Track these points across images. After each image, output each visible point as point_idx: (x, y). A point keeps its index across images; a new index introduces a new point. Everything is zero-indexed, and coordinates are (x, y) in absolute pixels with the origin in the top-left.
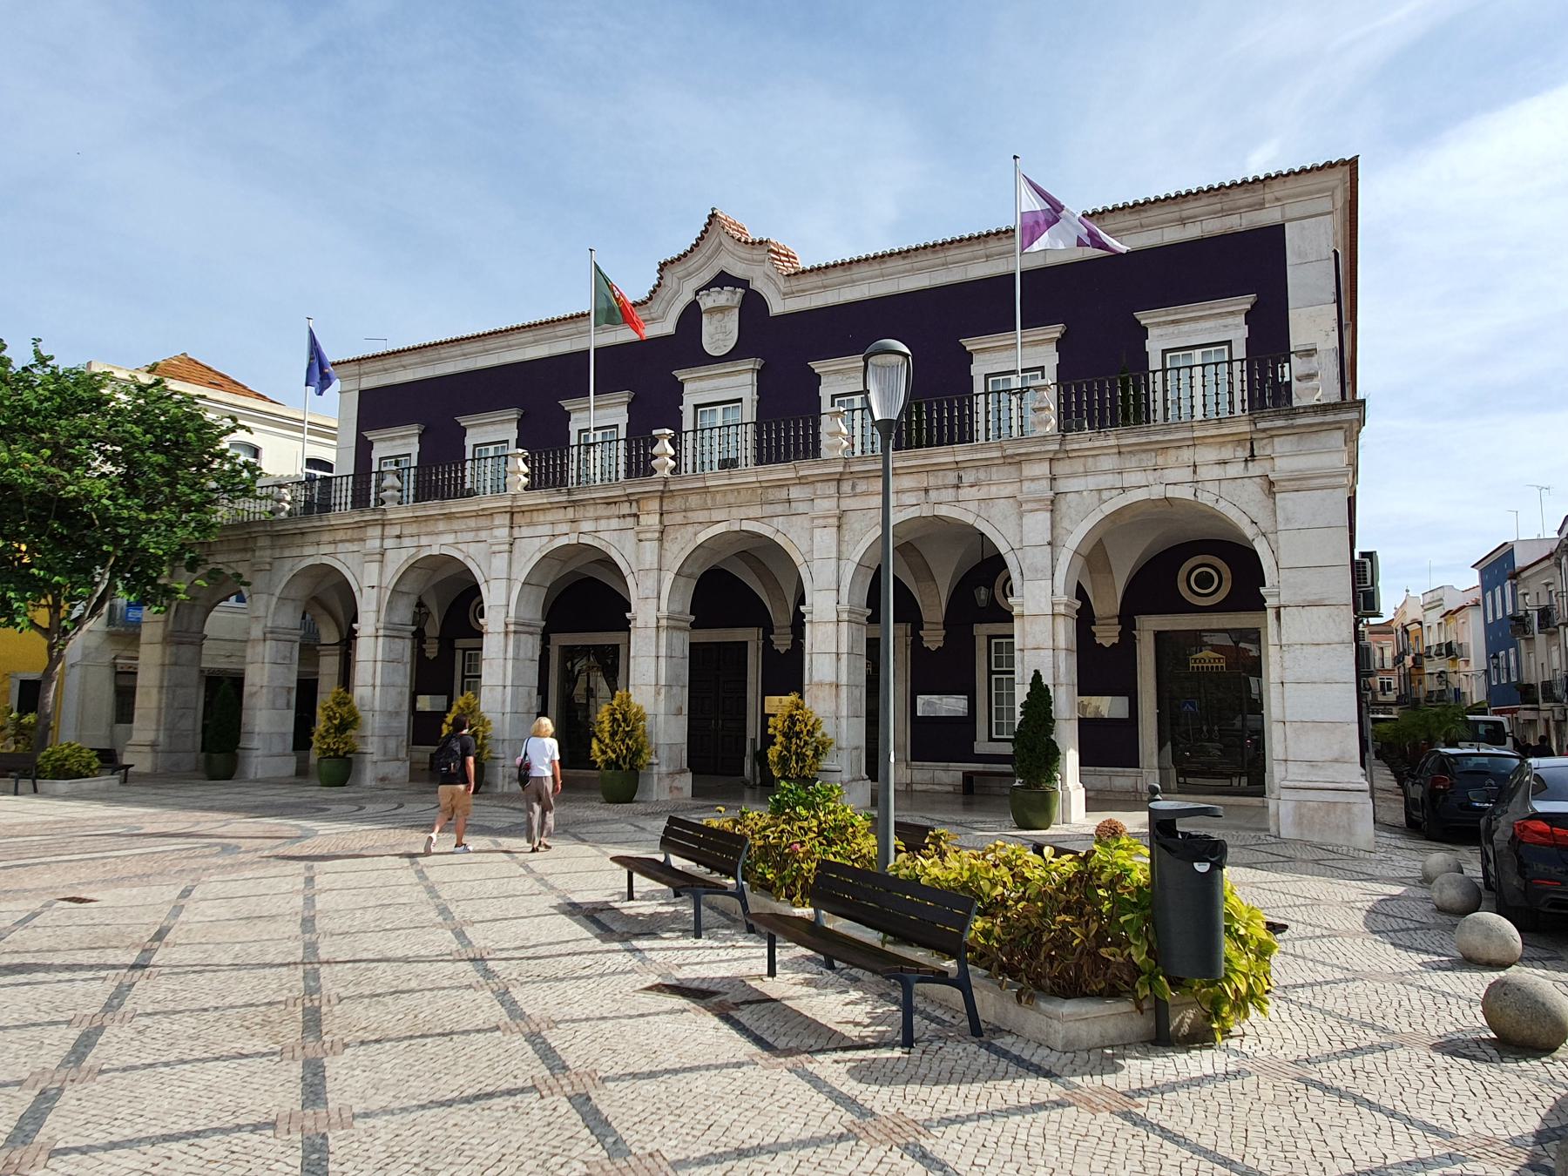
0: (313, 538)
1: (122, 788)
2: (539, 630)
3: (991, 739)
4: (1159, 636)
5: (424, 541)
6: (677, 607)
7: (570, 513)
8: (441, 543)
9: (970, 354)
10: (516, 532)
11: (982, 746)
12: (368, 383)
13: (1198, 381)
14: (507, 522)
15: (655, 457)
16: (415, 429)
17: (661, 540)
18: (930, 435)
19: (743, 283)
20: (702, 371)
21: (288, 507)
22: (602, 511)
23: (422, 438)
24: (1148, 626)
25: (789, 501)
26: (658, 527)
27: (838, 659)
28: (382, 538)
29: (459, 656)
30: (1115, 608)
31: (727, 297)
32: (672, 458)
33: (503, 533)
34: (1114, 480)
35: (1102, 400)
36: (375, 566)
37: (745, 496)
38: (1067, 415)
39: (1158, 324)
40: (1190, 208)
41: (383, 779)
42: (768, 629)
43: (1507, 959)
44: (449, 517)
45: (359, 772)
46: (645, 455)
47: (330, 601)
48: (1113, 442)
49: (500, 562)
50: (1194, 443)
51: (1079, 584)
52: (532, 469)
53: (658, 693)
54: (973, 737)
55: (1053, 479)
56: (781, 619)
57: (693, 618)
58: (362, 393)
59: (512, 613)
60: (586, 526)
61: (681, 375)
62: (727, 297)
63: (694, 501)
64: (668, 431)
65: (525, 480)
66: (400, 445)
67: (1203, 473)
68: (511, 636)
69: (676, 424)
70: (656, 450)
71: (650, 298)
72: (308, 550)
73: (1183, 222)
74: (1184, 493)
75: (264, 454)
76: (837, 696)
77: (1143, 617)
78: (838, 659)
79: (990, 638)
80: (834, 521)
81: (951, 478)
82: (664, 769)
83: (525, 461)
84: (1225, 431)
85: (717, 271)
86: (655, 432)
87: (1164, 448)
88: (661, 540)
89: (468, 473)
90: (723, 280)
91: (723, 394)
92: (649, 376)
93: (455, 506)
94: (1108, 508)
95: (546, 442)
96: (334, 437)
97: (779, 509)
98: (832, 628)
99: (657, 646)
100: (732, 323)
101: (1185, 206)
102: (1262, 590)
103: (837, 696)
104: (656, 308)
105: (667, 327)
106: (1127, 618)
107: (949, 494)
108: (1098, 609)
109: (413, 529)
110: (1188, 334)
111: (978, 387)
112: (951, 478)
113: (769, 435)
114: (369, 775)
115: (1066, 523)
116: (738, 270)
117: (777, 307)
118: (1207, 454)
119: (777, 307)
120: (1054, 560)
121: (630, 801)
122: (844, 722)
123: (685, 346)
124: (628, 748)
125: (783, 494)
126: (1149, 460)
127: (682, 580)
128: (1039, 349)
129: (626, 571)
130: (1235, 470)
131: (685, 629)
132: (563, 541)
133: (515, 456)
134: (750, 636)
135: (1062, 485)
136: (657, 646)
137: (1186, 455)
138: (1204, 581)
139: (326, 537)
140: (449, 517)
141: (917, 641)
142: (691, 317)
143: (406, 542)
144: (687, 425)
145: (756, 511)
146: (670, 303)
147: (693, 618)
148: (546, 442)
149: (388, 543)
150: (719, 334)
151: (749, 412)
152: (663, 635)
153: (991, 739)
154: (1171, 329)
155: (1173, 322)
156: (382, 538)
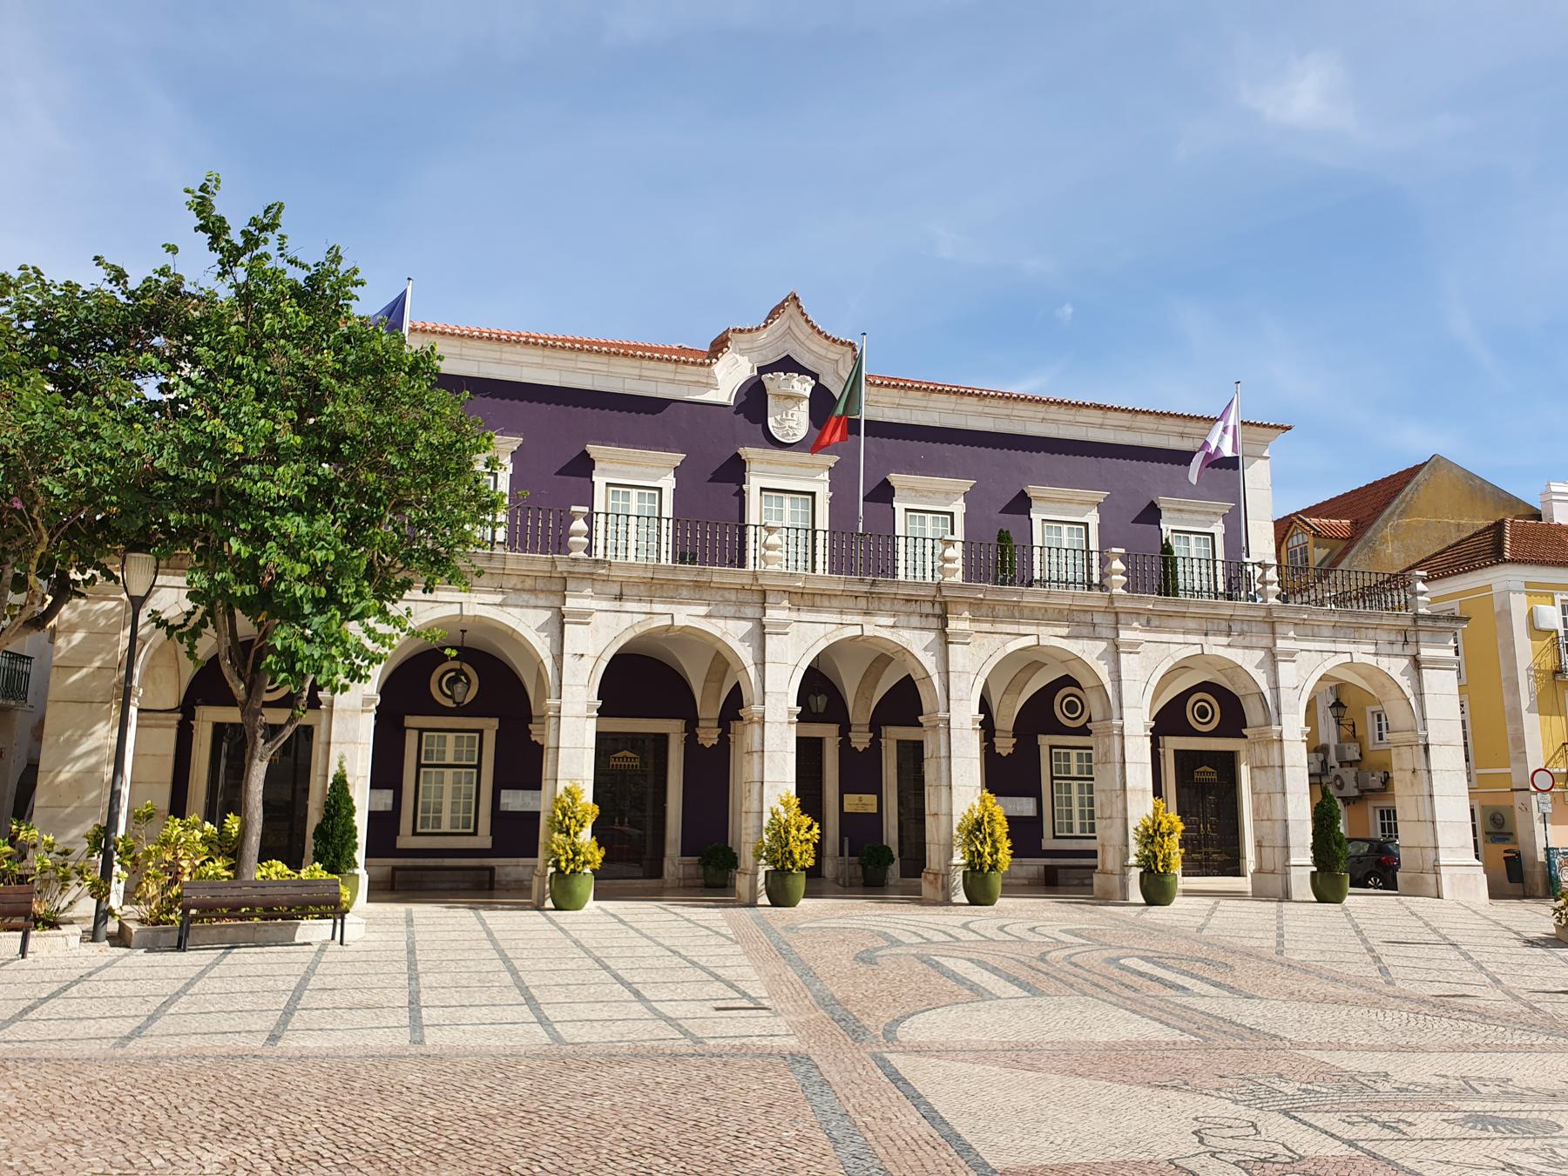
2: (701, 724)
3: (415, 833)
4: (1178, 754)
11: (1048, 843)
13: (632, 529)
18: (534, 536)
24: (893, 735)
25: (1094, 625)
29: (411, 739)
30: (716, 713)
35: (535, 527)
42: (692, 723)
54: (396, 831)
56: (709, 710)
77: (889, 729)
79: (1052, 747)
86: (574, 508)
93: (1012, 594)
106: (876, 726)
108: (998, 725)
125: (1088, 618)
134: (673, 729)
138: (1203, 713)
144: (599, 506)
153: (415, 833)
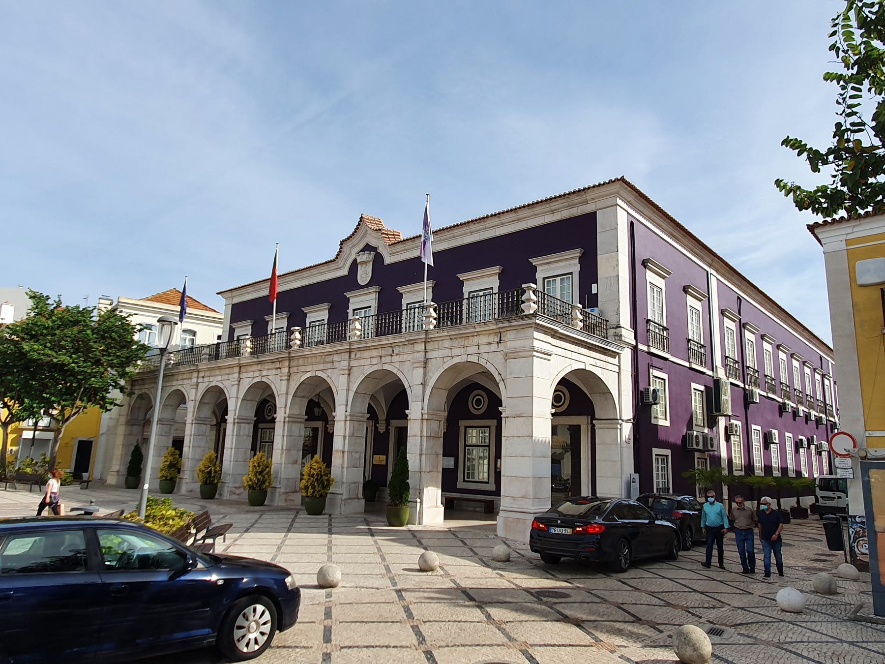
0: (176, 377)
1: (84, 491)
3: (464, 481)
5: (211, 379)
6: (296, 411)
7: (259, 367)
8: (216, 381)
9: (462, 282)
10: (353, 363)
12: (236, 300)
14: (347, 357)
15: (523, 302)
16: (326, 306)
17: (288, 380)
19: (375, 249)
20: (356, 293)
21: (358, 333)
22: (271, 366)
23: (501, 276)
26: (423, 359)
27: (345, 439)
28: (198, 378)
31: (367, 257)
32: (435, 319)
33: (236, 375)
34: (450, 353)
36: (194, 390)
37: (318, 359)
38: (502, 311)
39: (541, 265)
40: (554, 205)
41: (191, 491)
43: (427, 568)
44: (219, 368)
45: (179, 488)
46: (518, 301)
47: (217, 405)
48: (446, 334)
49: (343, 379)
50: (478, 334)
51: (369, 404)
52: (439, 315)
53: (282, 453)
55: (426, 351)
57: (369, 415)
58: (233, 305)
59: (349, 410)
60: (265, 373)
61: (348, 295)
62: (367, 257)
63: (301, 361)
64: (297, 328)
65: (434, 322)
66: (244, 330)
67: (484, 349)
68: (425, 422)
69: (304, 327)
70: (292, 337)
71: (337, 258)
72: (174, 383)
73: (553, 212)
74: (474, 359)
75: (197, 334)
76: (343, 456)
78: (345, 439)
80: (346, 372)
81: (390, 351)
82: (282, 490)
83: (435, 310)
84: (487, 328)
85: (364, 244)
86: (523, 286)
87: (467, 336)
88: (288, 380)
89: (404, 317)
90: (368, 248)
91: (364, 301)
92: (333, 293)
94: (446, 367)
95: (449, 298)
96: (221, 323)
97: (329, 365)
98: (343, 423)
99: (284, 430)
100: (369, 268)
101: (552, 204)
102: (500, 409)
103: (343, 456)
104: (340, 262)
105: (344, 272)
107: (388, 359)
109: (207, 374)
110: (554, 269)
111: (404, 307)
112: (390, 351)
113: (444, 310)
114: (279, 501)
115: (430, 374)
116: (373, 243)
117: (388, 260)
118: (484, 339)
119: (388, 260)
120: (424, 392)
121: (321, 514)
122: (345, 470)
123: (350, 282)
124: (258, 479)
126: (462, 342)
127: (298, 400)
128: (491, 278)
129: (498, 378)
130: (494, 347)
131: (301, 422)
132: (457, 360)
133: (430, 306)
135: (429, 355)
136: (284, 430)
137: (476, 340)
138: (478, 402)
139: (180, 377)
140: (219, 368)
141: (376, 428)
142: (354, 266)
143: (206, 379)
145: (321, 367)
146: (346, 260)
147: (369, 415)
148: (449, 298)
149: (200, 380)
150: (364, 275)
151: (373, 311)
152: (286, 425)
153: (464, 481)
154: (546, 267)
155: (547, 263)
156: (198, 378)
